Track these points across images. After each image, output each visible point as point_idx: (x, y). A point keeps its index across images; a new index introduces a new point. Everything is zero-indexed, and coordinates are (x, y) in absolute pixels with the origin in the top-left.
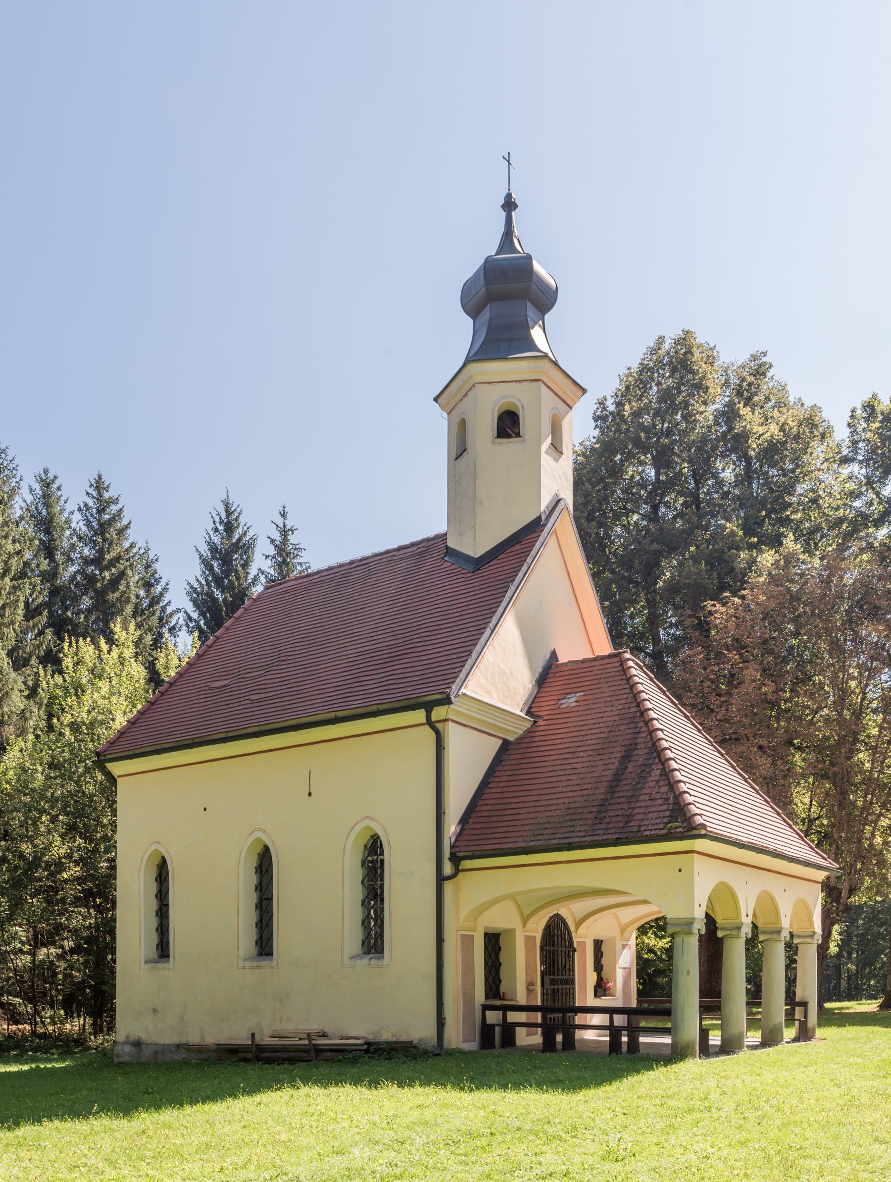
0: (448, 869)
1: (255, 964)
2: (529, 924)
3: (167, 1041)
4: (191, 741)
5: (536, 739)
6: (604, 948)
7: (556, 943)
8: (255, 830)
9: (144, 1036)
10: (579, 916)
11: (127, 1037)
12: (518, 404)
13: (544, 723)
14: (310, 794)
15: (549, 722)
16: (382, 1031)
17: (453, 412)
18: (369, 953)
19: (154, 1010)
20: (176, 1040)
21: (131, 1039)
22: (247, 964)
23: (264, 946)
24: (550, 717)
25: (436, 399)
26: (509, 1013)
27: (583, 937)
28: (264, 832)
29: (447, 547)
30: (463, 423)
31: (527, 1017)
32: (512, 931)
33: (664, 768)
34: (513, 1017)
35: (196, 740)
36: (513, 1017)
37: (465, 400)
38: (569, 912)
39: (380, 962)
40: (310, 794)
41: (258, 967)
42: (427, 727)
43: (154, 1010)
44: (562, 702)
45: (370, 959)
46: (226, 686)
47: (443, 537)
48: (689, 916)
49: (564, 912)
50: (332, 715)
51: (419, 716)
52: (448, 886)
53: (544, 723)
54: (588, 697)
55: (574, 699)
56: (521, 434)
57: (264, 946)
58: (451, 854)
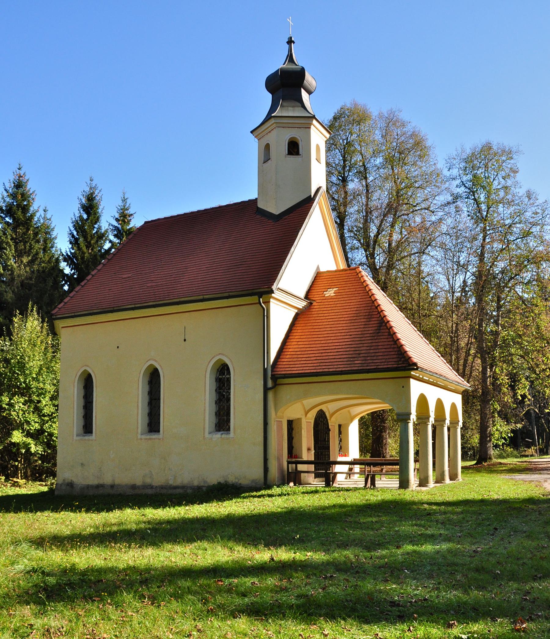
0: (270, 384)
1: (148, 437)
2: (308, 415)
3: (91, 483)
4: (112, 309)
5: (313, 313)
6: (294, 425)
7: (321, 425)
8: (149, 360)
9: (75, 480)
10: (332, 411)
11: (64, 480)
12: (298, 138)
13: (317, 304)
14: (185, 340)
15: (319, 304)
16: (229, 476)
17: (262, 140)
18: (219, 431)
19: (82, 464)
20: (96, 482)
21: (66, 481)
22: (143, 437)
23: (153, 425)
24: (320, 301)
25: (252, 132)
26: (298, 465)
27: (333, 423)
28: (156, 361)
29: (258, 208)
30: (267, 147)
31: (539, 484)
32: (299, 420)
33: (390, 332)
34: (301, 467)
35: (115, 309)
36: (301, 467)
37: (269, 134)
38: (328, 409)
39: (228, 436)
40: (185, 340)
41: (150, 439)
42: (259, 305)
43: (82, 464)
44: (325, 293)
45: (222, 434)
46: (130, 277)
47: (254, 202)
48: (407, 411)
49: (325, 410)
50: (201, 297)
51: (255, 299)
52: (270, 395)
53: (317, 304)
54: (341, 291)
55: (333, 292)
56: (301, 153)
57: (153, 425)
58: (272, 375)
